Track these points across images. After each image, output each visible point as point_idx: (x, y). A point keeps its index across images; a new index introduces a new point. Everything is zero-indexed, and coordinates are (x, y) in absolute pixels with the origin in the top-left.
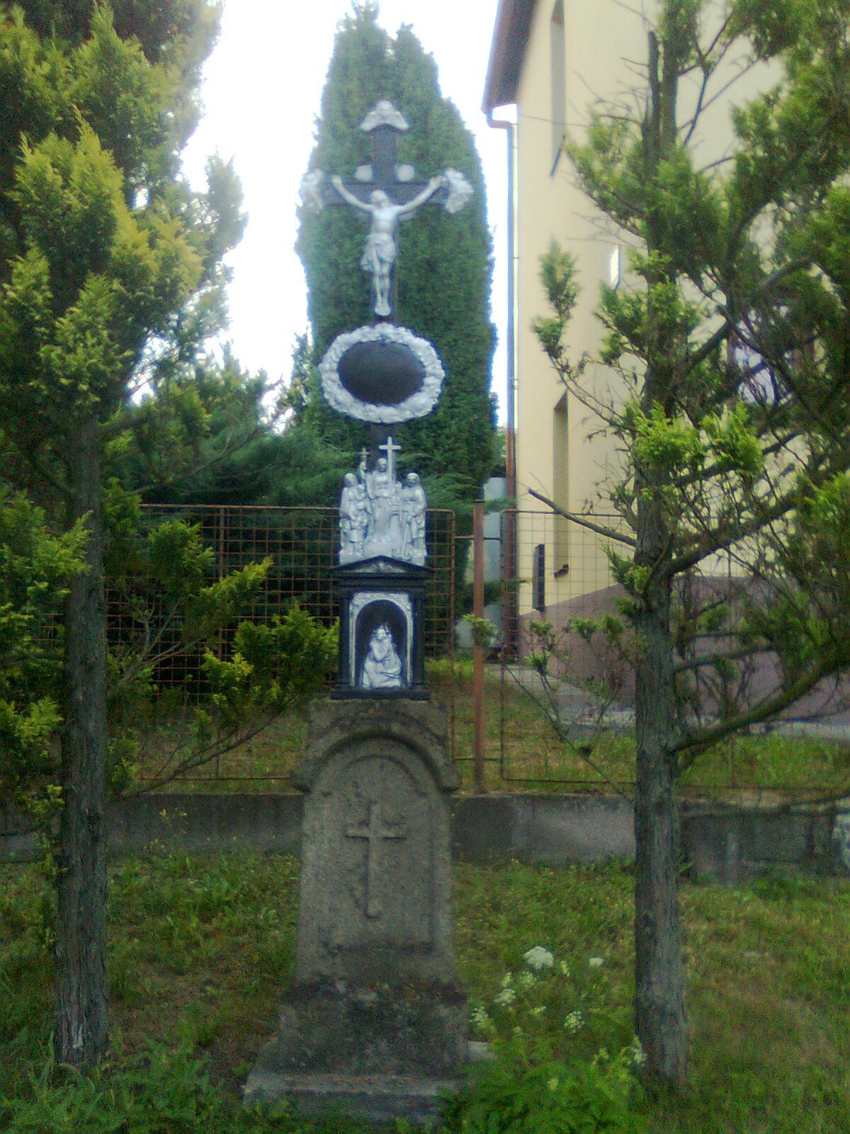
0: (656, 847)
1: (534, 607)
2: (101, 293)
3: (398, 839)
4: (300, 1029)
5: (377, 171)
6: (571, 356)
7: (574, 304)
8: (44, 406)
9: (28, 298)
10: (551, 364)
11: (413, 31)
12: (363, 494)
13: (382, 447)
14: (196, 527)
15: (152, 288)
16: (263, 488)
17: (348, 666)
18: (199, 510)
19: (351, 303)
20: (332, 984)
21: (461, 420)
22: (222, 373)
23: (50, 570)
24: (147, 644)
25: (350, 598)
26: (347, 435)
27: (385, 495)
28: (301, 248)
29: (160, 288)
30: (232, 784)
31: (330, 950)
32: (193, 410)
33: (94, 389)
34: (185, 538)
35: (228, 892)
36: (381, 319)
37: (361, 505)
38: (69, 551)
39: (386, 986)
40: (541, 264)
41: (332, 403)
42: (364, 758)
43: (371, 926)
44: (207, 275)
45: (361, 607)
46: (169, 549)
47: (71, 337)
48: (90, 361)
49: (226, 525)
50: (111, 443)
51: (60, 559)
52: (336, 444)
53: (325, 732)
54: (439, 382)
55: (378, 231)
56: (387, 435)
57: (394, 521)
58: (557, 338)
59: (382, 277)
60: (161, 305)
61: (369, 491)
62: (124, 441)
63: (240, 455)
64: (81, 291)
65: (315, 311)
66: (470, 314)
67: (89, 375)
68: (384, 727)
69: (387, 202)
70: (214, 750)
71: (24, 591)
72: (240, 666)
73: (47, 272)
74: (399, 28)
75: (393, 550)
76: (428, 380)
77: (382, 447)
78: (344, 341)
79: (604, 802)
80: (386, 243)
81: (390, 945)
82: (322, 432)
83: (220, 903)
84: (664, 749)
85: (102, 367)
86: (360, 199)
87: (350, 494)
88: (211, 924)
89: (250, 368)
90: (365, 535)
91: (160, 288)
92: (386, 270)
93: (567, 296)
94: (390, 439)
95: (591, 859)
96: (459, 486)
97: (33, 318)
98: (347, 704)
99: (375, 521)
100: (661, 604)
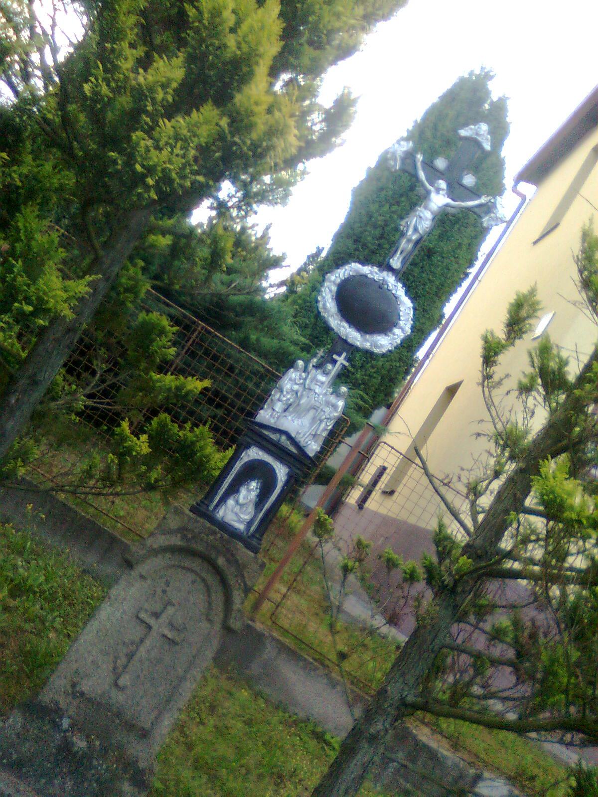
0: (352, 765)
1: (356, 502)
2: (210, 121)
3: (173, 642)
4: (18, 735)
5: (450, 168)
6: (498, 371)
7: (520, 338)
8: (111, 175)
9: (151, 90)
10: (481, 369)
11: (508, 102)
12: (302, 381)
13: (335, 356)
14: (176, 328)
15: (249, 142)
16: (237, 326)
17: (216, 493)
18: (185, 316)
19: (365, 245)
20: (61, 717)
21: (387, 361)
22: (257, 239)
23: (40, 300)
24: (89, 388)
25: (248, 447)
26: (311, 326)
27: (317, 391)
28: (357, 192)
29: (255, 146)
30: (91, 510)
31: (75, 692)
32: (222, 249)
33: (157, 187)
34: (162, 332)
35: (41, 584)
36: (390, 269)
37: (296, 387)
38: (65, 296)
39: (97, 743)
40: (515, 297)
41: (320, 305)
42: (183, 568)
43: (114, 693)
44: (290, 163)
45: (251, 458)
46: (148, 332)
47: (166, 139)
48: (169, 166)
49: (197, 337)
50: (153, 237)
51: (53, 297)
52: (300, 327)
53: (170, 532)
54: (402, 336)
55: (426, 208)
56: (344, 350)
57: (312, 413)
58: (496, 354)
59: (409, 241)
60: (247, 159)
61: (308, 381)
62: (164, 241)
63: (235, 299)
64: (194, 111)
65: (339, 237)
66: (436, 298)
67: (160, 175)
68: (213, 556)
69: (444, 192)
70: (88, 490)
71: (12, 304)
72: (142, 445)
73: (179, 81)
74: (501, 95)
75: (298, 433)
76: (397, 331)
77: (335, 356)
78: (353, 268)
79: (328, 676)
80: (427, 219)
81: (118, 715)
82: (295, 316)
83: (30, 590)
84: (402, 699)
85: (174, 175)
86: (427, 180)
87: (294, 375)
88: (14, 600)
89: (275, 248)
90: (285, 411)
91: (255, 146)
92: (414, 237)
93: (520, 330)
94: (344, 355)
95: (296, 711)
96: (361, 403)
97: (146, 106)
98: (197, 522)
99: (299, 405)
100: (463, 591)
